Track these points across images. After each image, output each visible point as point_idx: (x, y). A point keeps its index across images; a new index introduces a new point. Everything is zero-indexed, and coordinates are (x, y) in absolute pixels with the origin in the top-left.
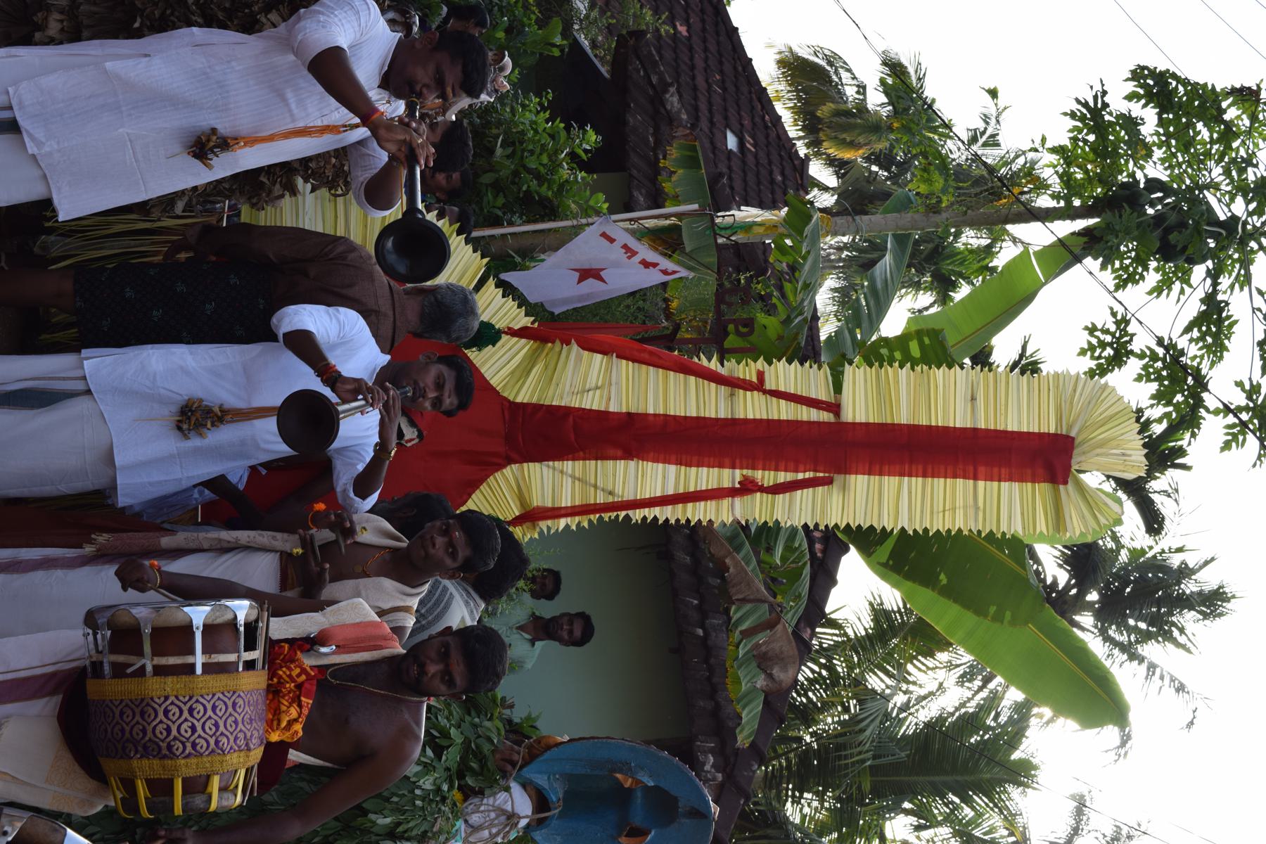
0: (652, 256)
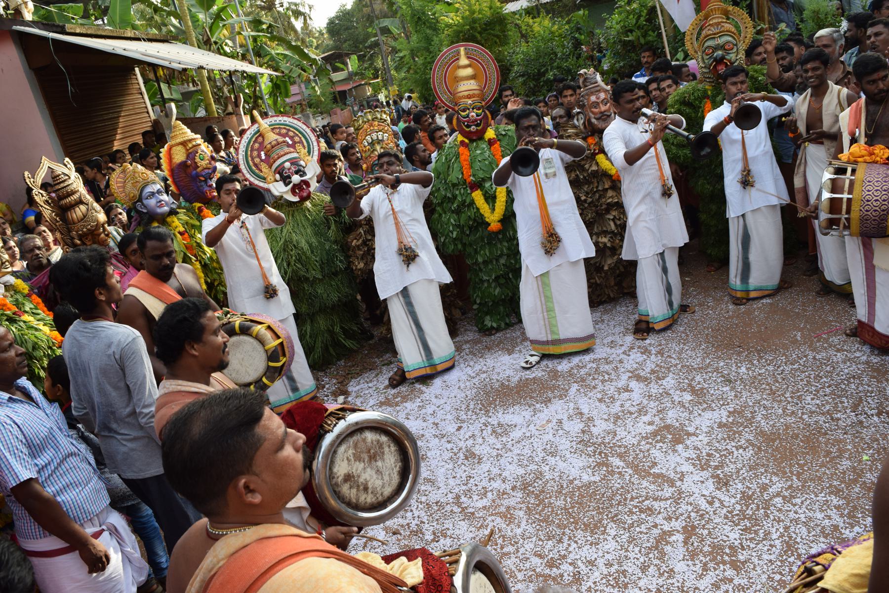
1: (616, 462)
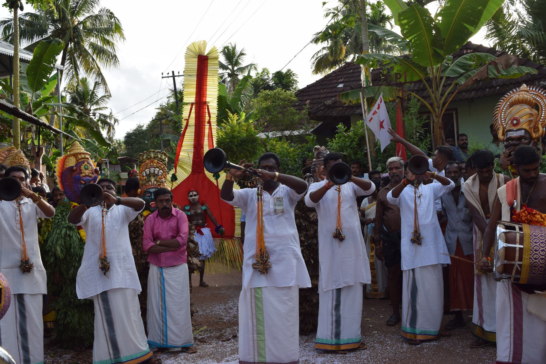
0: (376, 106)
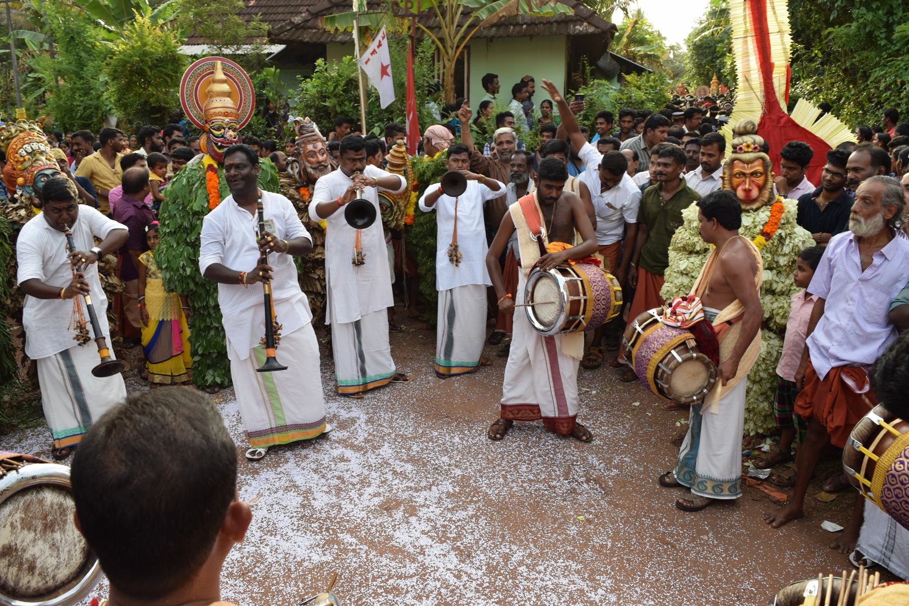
0: (376, 42)
1: (347, 538)
